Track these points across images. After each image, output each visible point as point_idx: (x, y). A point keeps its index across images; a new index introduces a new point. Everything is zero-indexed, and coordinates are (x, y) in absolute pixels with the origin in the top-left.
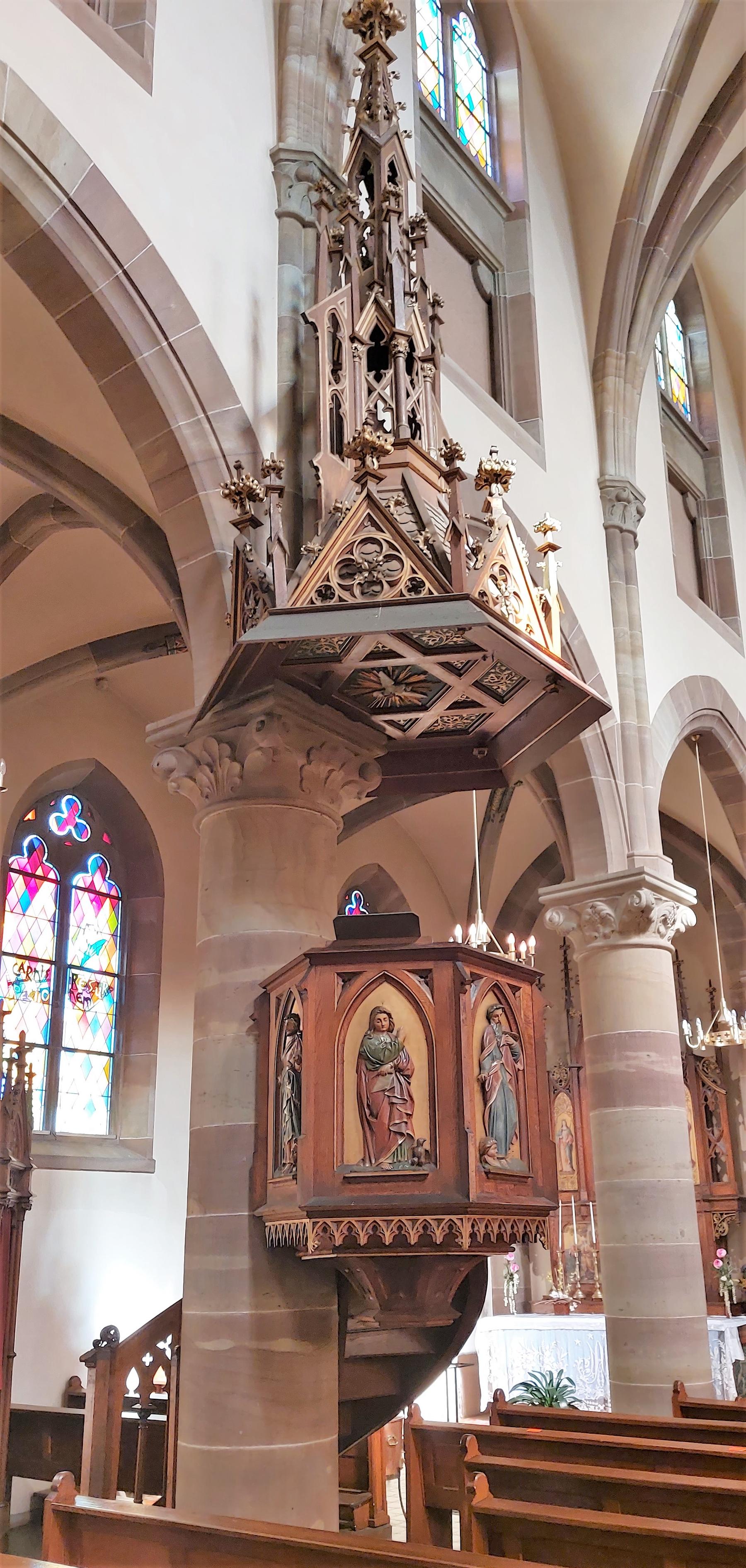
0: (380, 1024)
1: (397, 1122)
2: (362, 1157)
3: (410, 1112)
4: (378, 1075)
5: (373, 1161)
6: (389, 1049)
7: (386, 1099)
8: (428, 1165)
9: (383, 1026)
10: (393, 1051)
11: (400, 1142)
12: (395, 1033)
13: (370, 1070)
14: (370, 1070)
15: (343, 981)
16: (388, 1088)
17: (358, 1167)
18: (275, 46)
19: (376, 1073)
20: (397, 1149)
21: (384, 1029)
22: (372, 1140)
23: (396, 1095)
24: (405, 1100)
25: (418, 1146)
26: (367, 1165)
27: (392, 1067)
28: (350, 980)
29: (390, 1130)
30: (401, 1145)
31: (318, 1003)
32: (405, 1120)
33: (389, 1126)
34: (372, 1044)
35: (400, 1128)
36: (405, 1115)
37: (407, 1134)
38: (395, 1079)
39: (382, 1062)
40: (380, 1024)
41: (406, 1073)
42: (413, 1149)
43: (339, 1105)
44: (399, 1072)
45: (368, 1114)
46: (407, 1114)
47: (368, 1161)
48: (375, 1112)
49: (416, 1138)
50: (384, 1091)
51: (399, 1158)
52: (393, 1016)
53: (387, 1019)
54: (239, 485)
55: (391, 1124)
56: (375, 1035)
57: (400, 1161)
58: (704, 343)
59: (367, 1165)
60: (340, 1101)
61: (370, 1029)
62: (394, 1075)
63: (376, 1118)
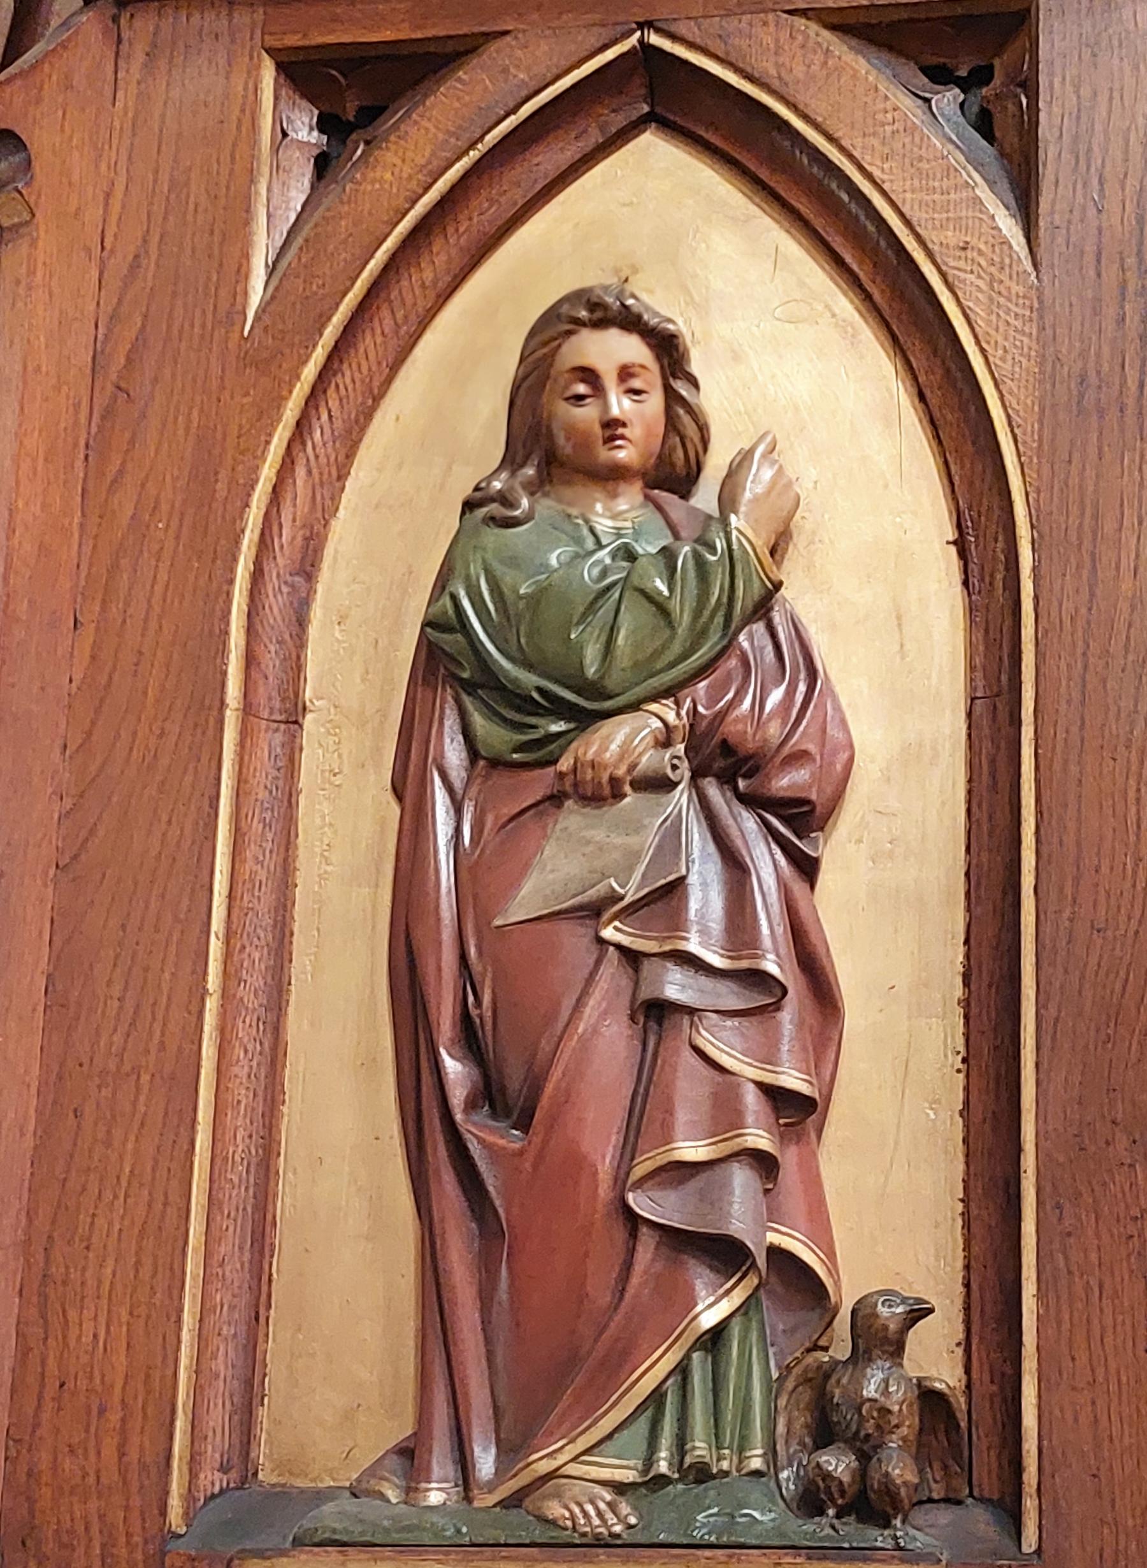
0: (587, 414)
1: (692, 1150)
2: (402, 1429)
3: (793, 1080)
4: (556, 799)
5: (485, 1463)
6: (649, 597)
7: (612, 968)
8: (944, 1516)
9: (612, 427)
10: (684, 619)
11: (709, 1319)
12: (705, 497)
13: (496, 763)
14: (496, 763)
15: (324, 124)
16: (631, 892)
17: (367, 1507)
18: (417, 1303)
19: (540, 783)
20: (682, 1370)
21: (624, 455)
22: (486, 1298)
23: (693, 946)
24: (756, 979)
25: (860, 1356)
26: (435, 1498)
27: (665, 741)
28: (371, 114)
29: (633, 1220)
30: (715, 1337)
31: (118, 264)
32: (759, 1139)
33: (621, 1183)
34: (513, 562)
35: (715, 1199)
36: (751, 1098)
37: (774, 1252)
38: (697, 838)
39: (594, 690)
40: (587, 414)
41: (785, 782)
42: (826, 1373)
43: (245, 1031)
44: (727, 779)
45: (458, 1096)
46: (774, 1094)
47: (441, 1463)
48: (514, 1079)
49: (847, 1300)
50: (594, 911)
51: (700, 1448)
52: (696, 367)
53: (651, 379)
54: (301, 342)
55: (638, 1172)
56: (546, 506)
57: (701, 1474)
58: (797, 328)
59: (435, 1498)
60: (251, 996)
61: (511, 461)
62: (681, 797)
63: (524, 1123)
